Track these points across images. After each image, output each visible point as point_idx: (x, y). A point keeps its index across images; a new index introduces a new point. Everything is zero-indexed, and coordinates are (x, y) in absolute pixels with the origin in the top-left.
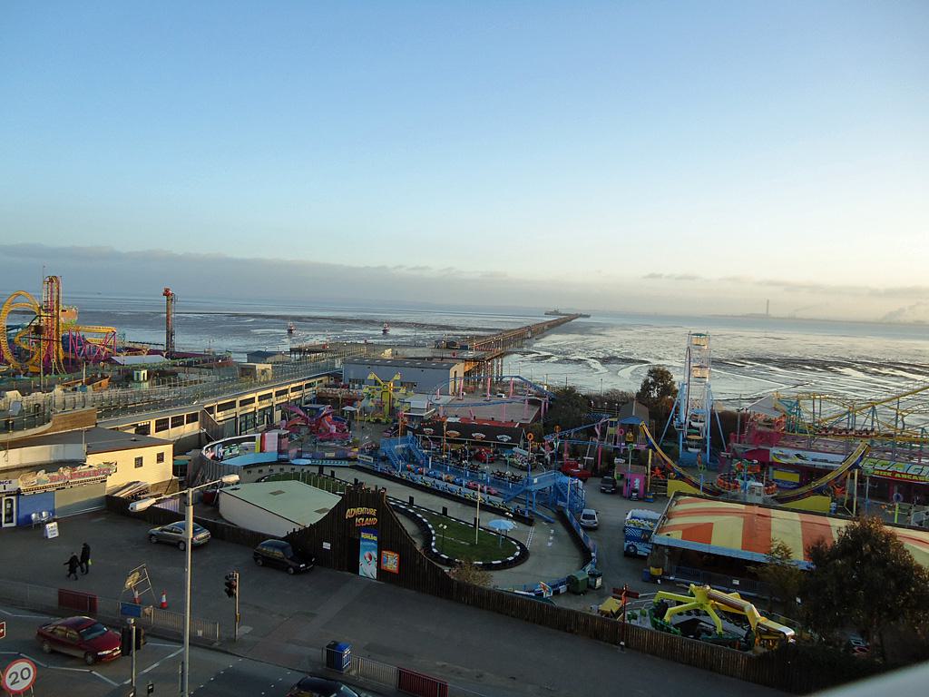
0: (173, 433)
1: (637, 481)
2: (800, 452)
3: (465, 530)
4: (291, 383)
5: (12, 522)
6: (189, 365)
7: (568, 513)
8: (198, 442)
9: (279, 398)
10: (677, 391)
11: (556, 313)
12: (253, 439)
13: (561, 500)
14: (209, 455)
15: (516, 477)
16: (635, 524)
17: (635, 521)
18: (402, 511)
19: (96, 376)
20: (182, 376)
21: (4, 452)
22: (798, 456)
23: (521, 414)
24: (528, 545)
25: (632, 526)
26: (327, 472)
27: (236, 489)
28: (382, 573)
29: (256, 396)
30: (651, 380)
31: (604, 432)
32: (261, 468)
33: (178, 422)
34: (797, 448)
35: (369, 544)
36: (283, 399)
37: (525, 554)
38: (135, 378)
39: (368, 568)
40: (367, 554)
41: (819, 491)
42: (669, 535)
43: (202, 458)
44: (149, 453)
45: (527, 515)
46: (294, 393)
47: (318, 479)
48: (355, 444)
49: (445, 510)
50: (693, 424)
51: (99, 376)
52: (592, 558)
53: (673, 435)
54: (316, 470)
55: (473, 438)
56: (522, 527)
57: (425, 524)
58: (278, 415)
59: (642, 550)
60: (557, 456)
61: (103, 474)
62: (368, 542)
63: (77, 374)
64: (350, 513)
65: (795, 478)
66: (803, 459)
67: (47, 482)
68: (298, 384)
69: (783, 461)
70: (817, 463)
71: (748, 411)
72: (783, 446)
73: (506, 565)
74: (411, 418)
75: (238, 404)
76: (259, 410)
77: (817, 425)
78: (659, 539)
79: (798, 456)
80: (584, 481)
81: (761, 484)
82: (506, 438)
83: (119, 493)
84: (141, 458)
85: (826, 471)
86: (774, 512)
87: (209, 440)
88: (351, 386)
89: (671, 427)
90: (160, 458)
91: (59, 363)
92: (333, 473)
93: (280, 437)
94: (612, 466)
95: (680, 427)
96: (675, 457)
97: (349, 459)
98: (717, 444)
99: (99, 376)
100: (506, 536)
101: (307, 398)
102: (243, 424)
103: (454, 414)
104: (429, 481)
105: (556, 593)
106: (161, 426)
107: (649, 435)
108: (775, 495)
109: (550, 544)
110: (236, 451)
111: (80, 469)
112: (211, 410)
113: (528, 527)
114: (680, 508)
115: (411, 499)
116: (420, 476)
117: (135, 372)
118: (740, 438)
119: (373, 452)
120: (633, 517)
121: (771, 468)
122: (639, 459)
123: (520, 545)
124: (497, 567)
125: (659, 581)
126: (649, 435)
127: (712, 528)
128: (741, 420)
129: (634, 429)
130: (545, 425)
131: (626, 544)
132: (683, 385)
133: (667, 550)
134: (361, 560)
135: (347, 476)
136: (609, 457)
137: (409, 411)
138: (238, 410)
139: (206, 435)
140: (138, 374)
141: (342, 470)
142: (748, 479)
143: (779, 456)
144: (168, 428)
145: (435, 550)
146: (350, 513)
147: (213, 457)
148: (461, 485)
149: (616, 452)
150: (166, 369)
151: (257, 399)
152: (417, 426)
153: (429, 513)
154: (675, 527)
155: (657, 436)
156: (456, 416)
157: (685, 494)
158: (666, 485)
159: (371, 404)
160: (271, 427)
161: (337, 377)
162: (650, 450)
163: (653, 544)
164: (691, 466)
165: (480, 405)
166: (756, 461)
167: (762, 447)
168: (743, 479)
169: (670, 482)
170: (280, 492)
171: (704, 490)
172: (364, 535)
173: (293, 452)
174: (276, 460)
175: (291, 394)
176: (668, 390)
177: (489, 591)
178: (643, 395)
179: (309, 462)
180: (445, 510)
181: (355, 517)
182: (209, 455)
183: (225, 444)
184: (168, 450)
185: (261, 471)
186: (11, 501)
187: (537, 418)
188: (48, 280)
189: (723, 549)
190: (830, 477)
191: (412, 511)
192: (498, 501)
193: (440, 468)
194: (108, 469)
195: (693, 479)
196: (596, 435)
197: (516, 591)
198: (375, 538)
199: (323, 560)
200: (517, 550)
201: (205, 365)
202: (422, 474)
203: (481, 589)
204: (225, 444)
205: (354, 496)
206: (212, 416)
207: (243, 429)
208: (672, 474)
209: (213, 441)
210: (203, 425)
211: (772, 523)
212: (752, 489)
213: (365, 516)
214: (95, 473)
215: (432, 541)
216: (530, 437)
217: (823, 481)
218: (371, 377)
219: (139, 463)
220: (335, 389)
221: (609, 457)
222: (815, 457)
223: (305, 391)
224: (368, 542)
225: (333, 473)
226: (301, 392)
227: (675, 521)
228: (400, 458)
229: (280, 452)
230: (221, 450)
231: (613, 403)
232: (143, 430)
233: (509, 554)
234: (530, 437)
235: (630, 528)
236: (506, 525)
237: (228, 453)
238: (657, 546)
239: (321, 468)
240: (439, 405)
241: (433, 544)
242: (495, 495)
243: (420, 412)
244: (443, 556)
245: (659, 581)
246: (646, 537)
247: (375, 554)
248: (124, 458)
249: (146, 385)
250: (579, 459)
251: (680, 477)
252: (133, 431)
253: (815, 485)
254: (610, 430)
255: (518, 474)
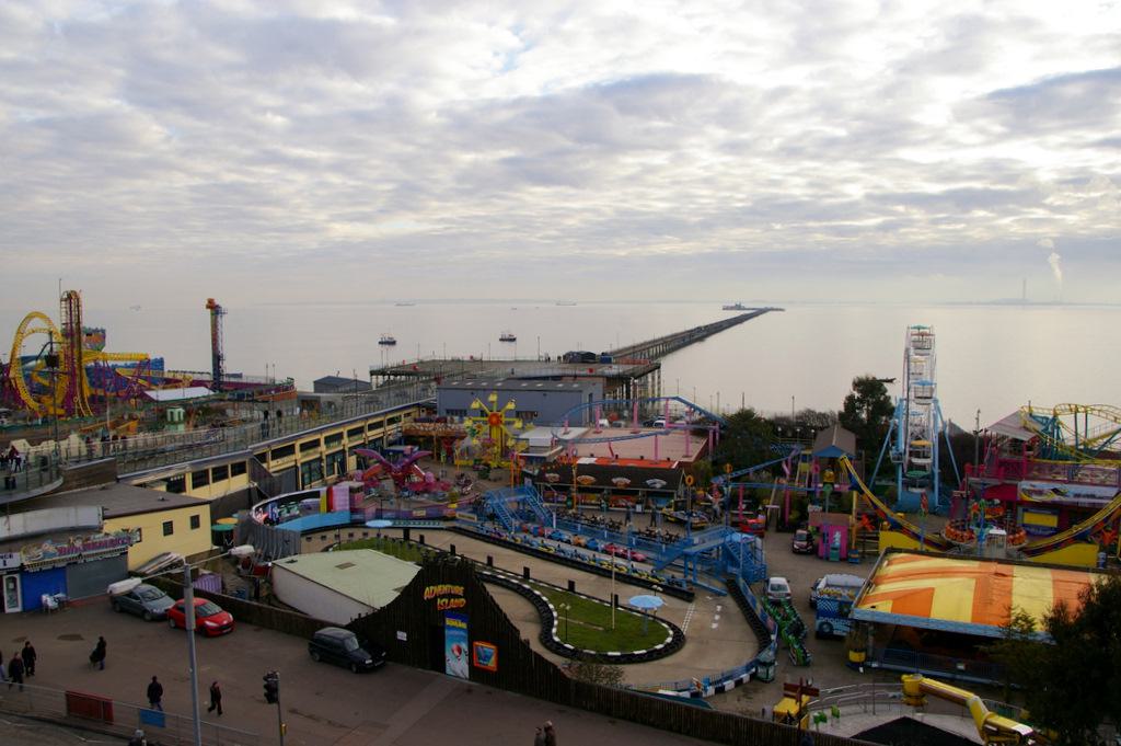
0: (215, 490)
1: (838, 536)
2: (1057, 486)
3: (595, 609)
4: (367, 419)
5: (17, 606)
6: (240, 398)
7: (741, 582)
8: (246, 499)
9: (305, 453)
10: (893, 409)
11: (738, 307)
12: (316, 495)
13: (732, 565)
14: (260, 518)
15: (671, 536)
16: (829, 595)
17: (830, 590)
18: (516, 587)
19: (123, 418)
20: (230, 412)
21: (4, 519)
22: (1056, 491)
23: (676, 449)
24: (685, 628)
25: (826, 596)
26: (414, 536)
27: (292, 562)
28: (476, 672)
29: (345, 430)
30: (857, 395)
31: (794, 468)
32: (324, 534)
33: (220, 474)
34: (1054, 481)
35: (457, 633)
36: (357, 440)
37: (680, 639)
38: (169, 419)
39: (457, 665)
40: (454, 646)
41: (1081, 538)
42: (873, 607)
43: (250, 520)
44: (181, 518)
45: (685, 587)
46: (280, 461)
47: (397, 548)
48: (453, 499)
49: (571, 584)
50: (915, 460)
51: (126, 417)
52: (771, 641)
53: (889, 470)
54: (400, 534)
55: (616, 485)
56: (676, 603)
57: (545, 604)
58: (352, 462)
59: (840, 628)
60: (732, 502)
61: (123, 543)
62: (456, 627)
63: (103, 418)
64: (429, 592)
65: (1052, 521)
66: (1062, 494)
67: (54, 555)
68: (379, 419)
69: (1036, 498)
70: (1082, 500)
71: (989, 433)
72: (1034, 479)
73: (653, 656)
74: (529, 460)
75: (297, 448)
76: (303, 464)
77: (1082, 447)
78: (862, 611)
79: (1056, 491)
80: (762, 536)
81: (1003, 532)
82: (659, 484)
83: (147, 568)
84: (171, 523)
85: (1094, 509)
86: (1017, 570)
87: (263, 497)
88: (449, 418)
89: (886, 460)
90: (195, 522)
91: (83, 402)
92: (422, 537)
93: (352, 490)
94: (804, 516)
95: (898, 459)
96: (891, 500)
97: (445, 519)
98: (949, 478)
99: (126, 417)
100: (655, 617)
101: (391, 438)
102: (306, 476)
103: (588, 452)
104: (553, 545)
105: (720, 690)
106: (200, 480)
107: (853, 472)
108: (1024, 544)
109: (714, 626)
110: (295, 511)
111: (98, 537)
112: (262, 457)
113: (686, 604)
114: (894, 568)
115: (527, 570)
116: (539, 540)
117: (169, 411)
118: (979, 470)
119: (477, 507)
120: (827, 585)
121: (1020, 509)
122: (840, 504)
123: (674, 628)
124: (641, 659)
125: (861, 670)
126: (853, 472)
127: (933, 594)
128: (980, 447)
129: (833, 463)
130: (714, 463)
131: (818, 622)
132: (901, 400)
133: (872, 628)
134: (448, 654)
135: (439, 541)
136: (800, 505)
137: (527, 451)
138: (299, 457)
139: (259, 491)
140: (172, 413)
141: (436, 533)
142: (985, 526)
143: (1030, 493)
144: (208, 483)
145: (556, 639)
146: (429, 592)
147: (267, 520)
148: (596, 550)
149: (811, 497)
150: (211, 405)
151: (345, 435)
152: (537, 472)
153: (550, 589)
154: (885, 596)
155: (867, 472)
156: (592, 456)
157: (900, 551)
158: (877, 539)
159: (475, 442)
160: (343, 474)
161: (431, 409)
162: (855, 493)
163: (852, 619)
164: (911, 511)
165: (622, 438)
166: (997, 501)
167: (1008, 482)
168: (978, 526)
169: (882, 534)
170: (348, 565)
171: (928, 542)
172: (449, 622)
173: (371, 509)
174: (347, 521)
175: (369, 434)
176: (884, 408)
177: (618, 693)
178: (848, 417)
179: (388, 523)
180: (571, 584)
181: (436, 598)
182: (260, 518)
183: (280, 502)
184: (204, 513)
185: (324, 538)
186: (14, 580)
187: (703, 454)
188: (65, 296)
189: (946, 623)
190: (1098, 517)
191: (527, 586)
192: (645, 570)
193: (567, 527)
194: (127, 538)
195: (914, 529)
196: (783, 474)
197: (661, 692)
198: (464, 625)
199: (400, 655)
200: (668, 635)
201: (259, 398)
202: (543, 536)
203: (608, 690)
204: (280, 502)
205: (436, 568)
206: (265, 465)
207: (307, 481)
208: (885, 523)
209: (266, 498)
210: (253, 477)
211: (1014, 584)
212: (991, 538)
213: (450, 596)
214: (113, 543)
215: (552, 626)
216: (689, 480)
217: (1088, 524)
218: (475, 405)
219: (168, 529)
220: (427, 424)
221: (800, 505)
222: (1078, 492)
223: (388, 428)
224: (456, 627)
225: (422, 537)
226: (381, 430)
227: (884, 588)
228: (513, 516)
229: (353, 511)
230: (276, 511)
231: (802, 429)
232: (176, 486)
233: (657, 641)
234: (689, 480)
235: (823, 599)
236: (650, 601)
237: (285, 514)
238: (858, 624)
239: (407, 531)
240: (566, 441)
241: (554, 630)
242: (643, 561)
243: (541, 452)
244: (567, 646)
245: (861, 670)
246: (843, 610)
247: (464, 646)
248: (151, 524)
249: (181, 428)
250: (760, 508)
251: (896, 527)
252: (163, 488)
253: (1077, 529)
254: (803, 467)
255: (674, 531)
